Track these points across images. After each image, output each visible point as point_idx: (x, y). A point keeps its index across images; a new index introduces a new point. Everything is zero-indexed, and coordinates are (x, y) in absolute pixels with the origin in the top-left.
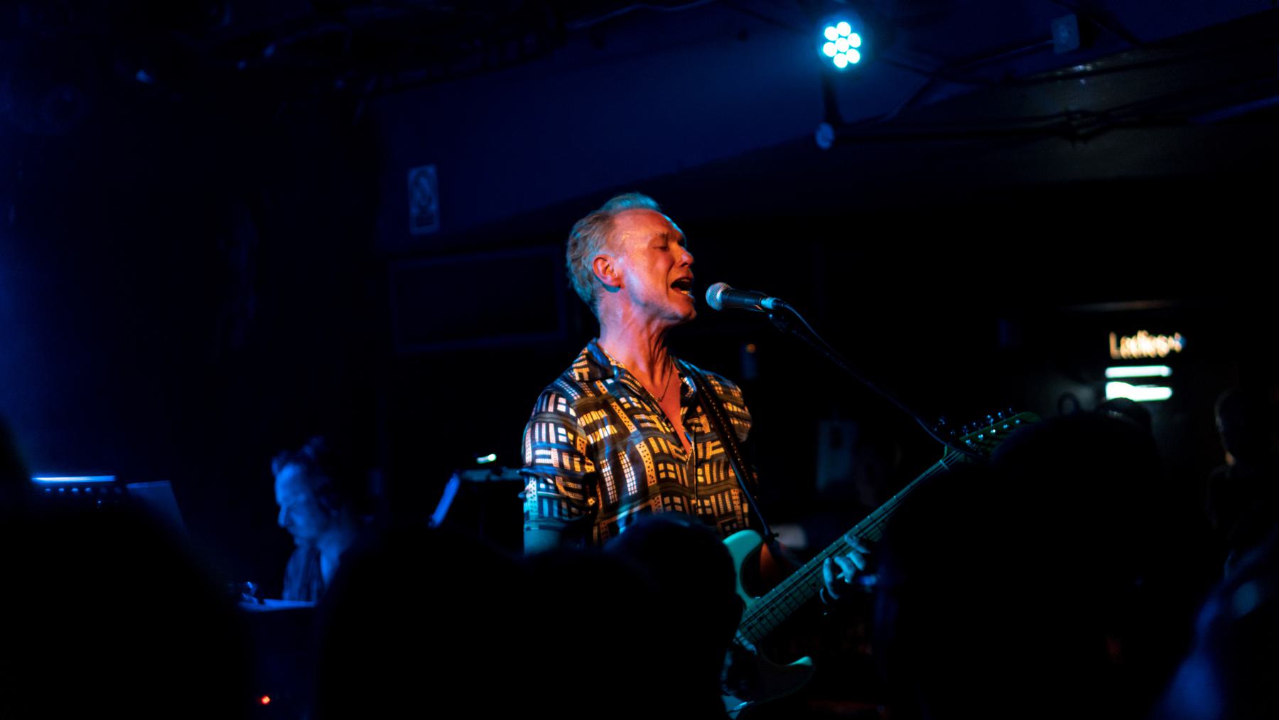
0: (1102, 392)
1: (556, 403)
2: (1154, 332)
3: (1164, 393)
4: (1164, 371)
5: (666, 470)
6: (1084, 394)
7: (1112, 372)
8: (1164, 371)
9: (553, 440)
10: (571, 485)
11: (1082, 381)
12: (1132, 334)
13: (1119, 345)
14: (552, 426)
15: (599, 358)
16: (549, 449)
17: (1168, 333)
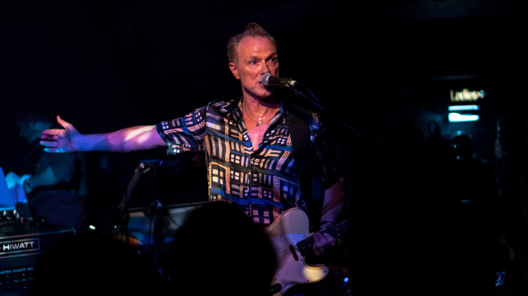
0: (446, 118)
2: (471, 90)
3: (475, 118)
4: (475, 107)
5: (235, 159)
6: (438, 118)
7: (452, 108)
8: (475, 107)
10: (236, 136)
11: (437, 112)
12: (461, 90)
13: (454, 96)
17: (477, 90)
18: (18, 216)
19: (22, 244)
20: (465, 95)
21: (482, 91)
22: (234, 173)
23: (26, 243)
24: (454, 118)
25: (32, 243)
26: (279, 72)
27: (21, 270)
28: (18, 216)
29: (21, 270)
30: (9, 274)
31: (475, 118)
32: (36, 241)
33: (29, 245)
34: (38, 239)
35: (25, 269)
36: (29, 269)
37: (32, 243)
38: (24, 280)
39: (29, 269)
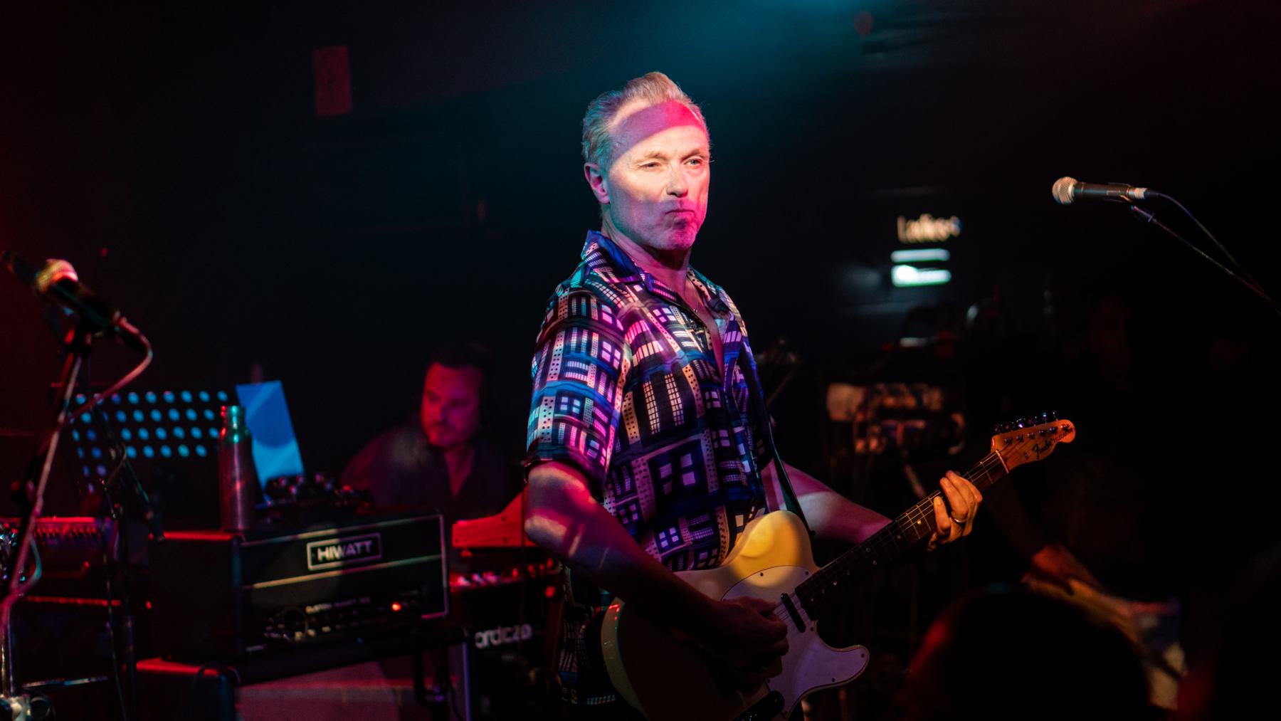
1: (600, 311)
3: (939, 276)
7: (900, 255)
9: (594, 353)
12: (915, 217)
13: (905, 229)
14: (595, 338)
15: (620, 260)
16: (588, 363)
18: (329, 486)
19: (351, 546)
20: (926, 228)
21: (954, 218)
22: (213, 396)
23: (358, 545)
24: (905, 276)
25: (368, 544)
26: (703, 274)
27: (348, 603)
28: (329, 486)
29: (348, 603)
30: (327, 611)
31: (939, 276)
32: (375, 540)
33: (363, 548)
34: (311, 567)
35: (354, 601)
36: (363, 601)
37: (368, 544)
38: (354, 624)
39: (363, 601)
